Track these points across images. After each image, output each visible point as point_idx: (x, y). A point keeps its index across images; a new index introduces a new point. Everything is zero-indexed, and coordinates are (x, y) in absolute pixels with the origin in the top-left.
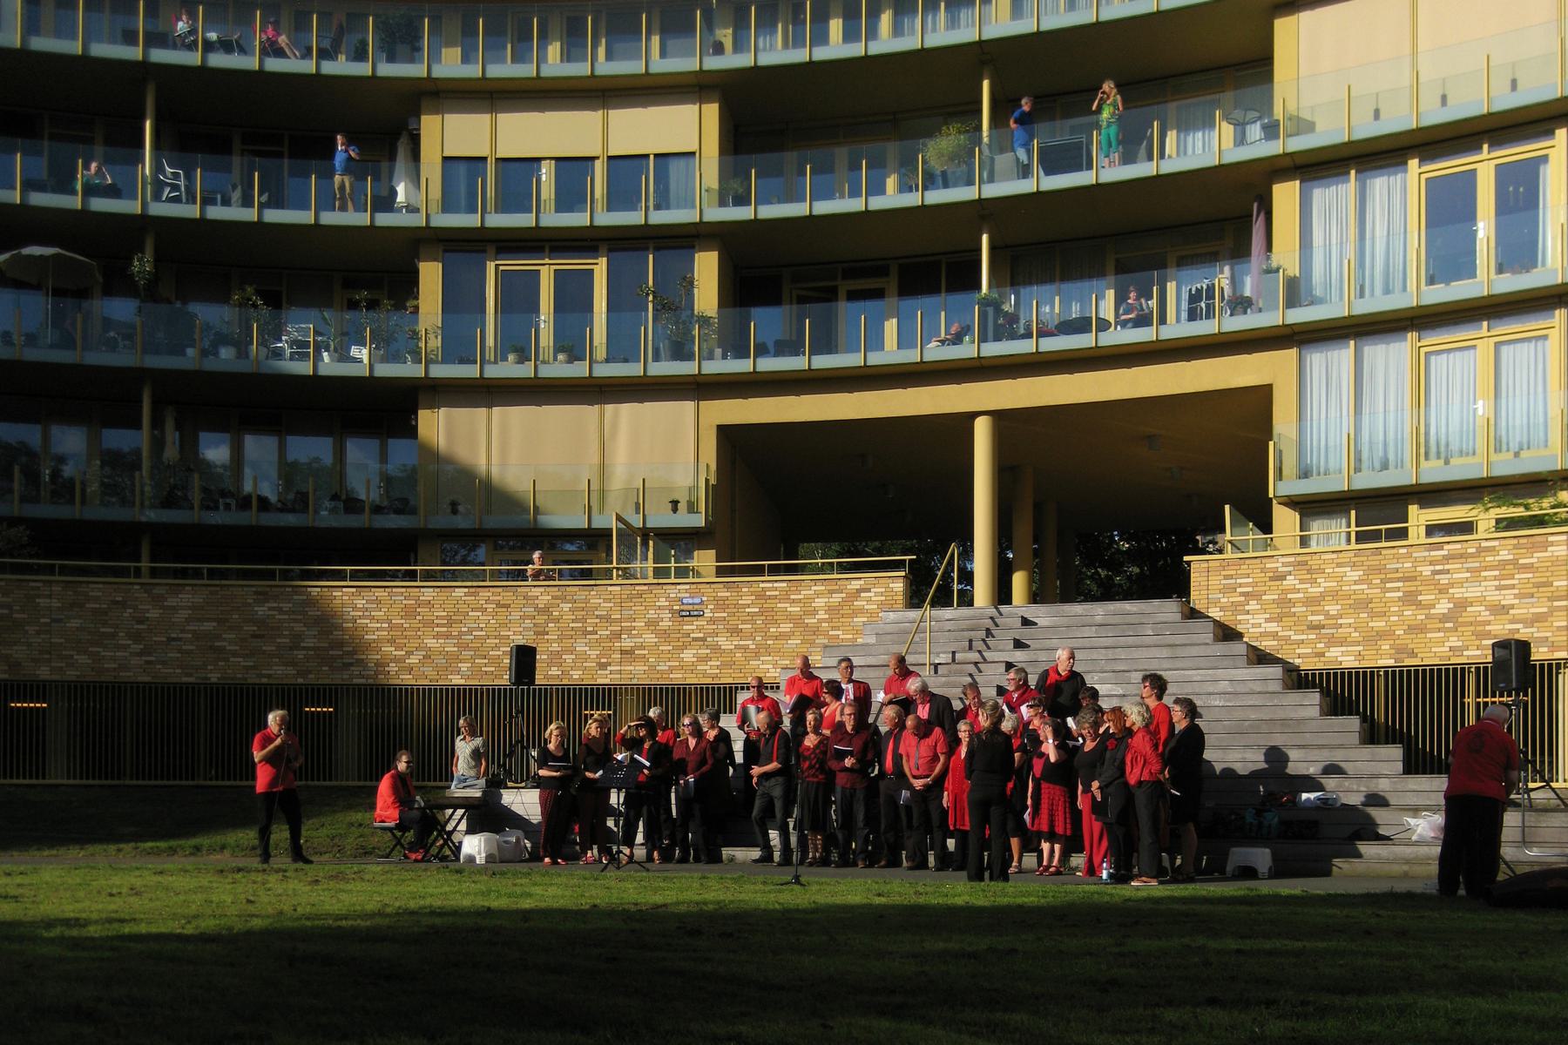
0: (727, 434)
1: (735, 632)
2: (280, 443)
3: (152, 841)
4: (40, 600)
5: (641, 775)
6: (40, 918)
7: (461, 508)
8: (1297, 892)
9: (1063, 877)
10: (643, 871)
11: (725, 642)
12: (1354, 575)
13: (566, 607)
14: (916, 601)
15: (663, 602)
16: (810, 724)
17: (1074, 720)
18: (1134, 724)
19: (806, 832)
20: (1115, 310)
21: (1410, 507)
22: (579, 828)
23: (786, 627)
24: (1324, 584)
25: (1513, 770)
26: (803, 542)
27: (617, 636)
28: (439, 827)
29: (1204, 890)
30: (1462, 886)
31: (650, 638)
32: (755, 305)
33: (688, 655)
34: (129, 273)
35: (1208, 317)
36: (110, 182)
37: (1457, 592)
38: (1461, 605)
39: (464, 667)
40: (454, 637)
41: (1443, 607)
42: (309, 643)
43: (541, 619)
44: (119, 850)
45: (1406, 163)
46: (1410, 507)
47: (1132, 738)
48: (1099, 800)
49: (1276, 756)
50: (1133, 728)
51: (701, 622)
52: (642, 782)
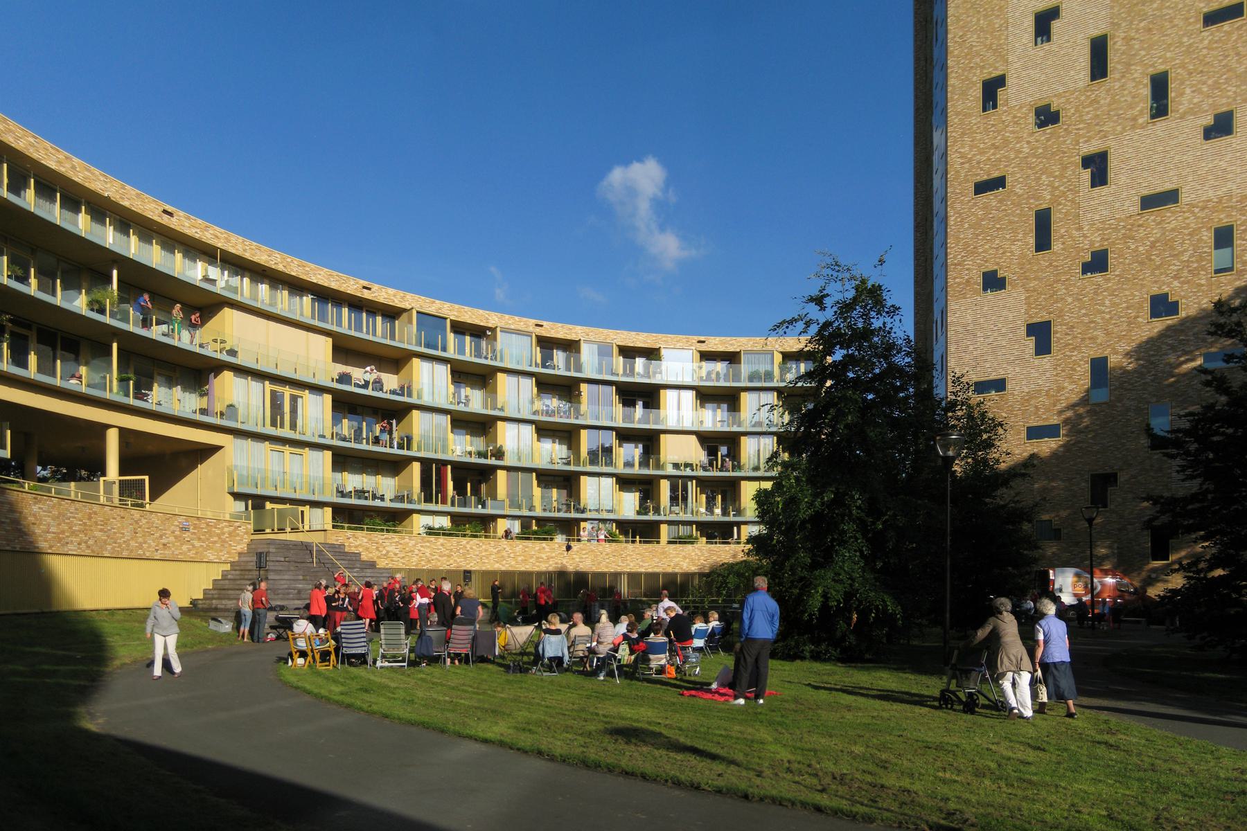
0: (18, 195)
1: (199, 539)
8: (1233, 717)
11: (197, 544)
12: (365, 540)
13: (144, 521)
15: (176, 523)
23: (215, 539)
24: (358, 543)
27: (161, 537)
31: (172, 539)
33: (185, 548)
35: (120, 500)
37: (387, 548)
38: (388, 552)
39: (109, 547)
40: (105, 532)
41: (384, 552)
42: (53, 529)
43: (136, 526)
45: (195, 261)
48: (604, 612)
51: (188, 534)
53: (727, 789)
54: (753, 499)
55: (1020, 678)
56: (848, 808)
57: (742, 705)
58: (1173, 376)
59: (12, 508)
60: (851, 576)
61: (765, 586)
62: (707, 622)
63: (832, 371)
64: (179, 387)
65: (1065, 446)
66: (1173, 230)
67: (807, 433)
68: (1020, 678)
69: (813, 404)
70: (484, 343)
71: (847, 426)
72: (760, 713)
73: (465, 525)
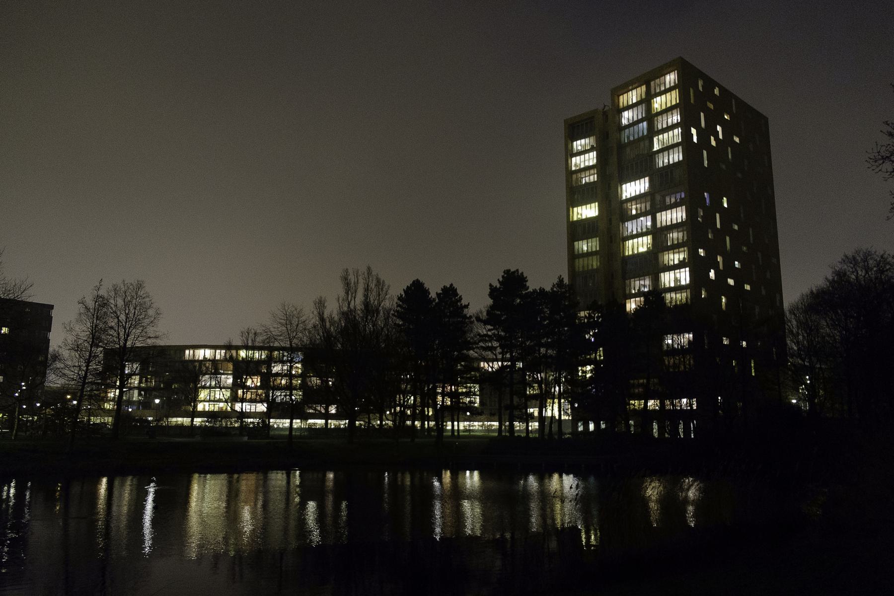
2: (230, 483)
3: (130, 500)
4: (250, 420)
5: (295, 426)
6: (285, 505)
7: (885, 182)
9: (565, 208)
10: (263, 342)
14: (506, 272)
16: (490, 330)
17: (470, 473)
18: (320, 304)
19: (808, 382)
20: (707, 76)
21: (498, 423)
22: (691, 436)
25: (627, 280)
26: (594, 182)
28: (374, 411)
29: (381, 323)
30: (757, 313)
32: (201, 411)
34: (490, 309)
36: (110, 419)
44: (200, 477)
46: (498, 423)
47: (833, 272)
49: (452, 285)
50: (679, 242)
52: (581, 431)
53: (837, 275)
54: (452, 285)
55: (332, 311)
56: (651, 382)
57: (534, 475)
58: (340, 321)
59: (726, 308)
60: (383, 328)
61: (240, 404)
62: (829, 321)
63: (807, 362)
64: (571, 476)
65: (665, 303)
66: (851, 263)
67: (491, 336)
68: (332, 311)
69: (737, 229)
70: (346, 309)
71: (875, 271)
72: (127, 315)
73: (526, 495)
